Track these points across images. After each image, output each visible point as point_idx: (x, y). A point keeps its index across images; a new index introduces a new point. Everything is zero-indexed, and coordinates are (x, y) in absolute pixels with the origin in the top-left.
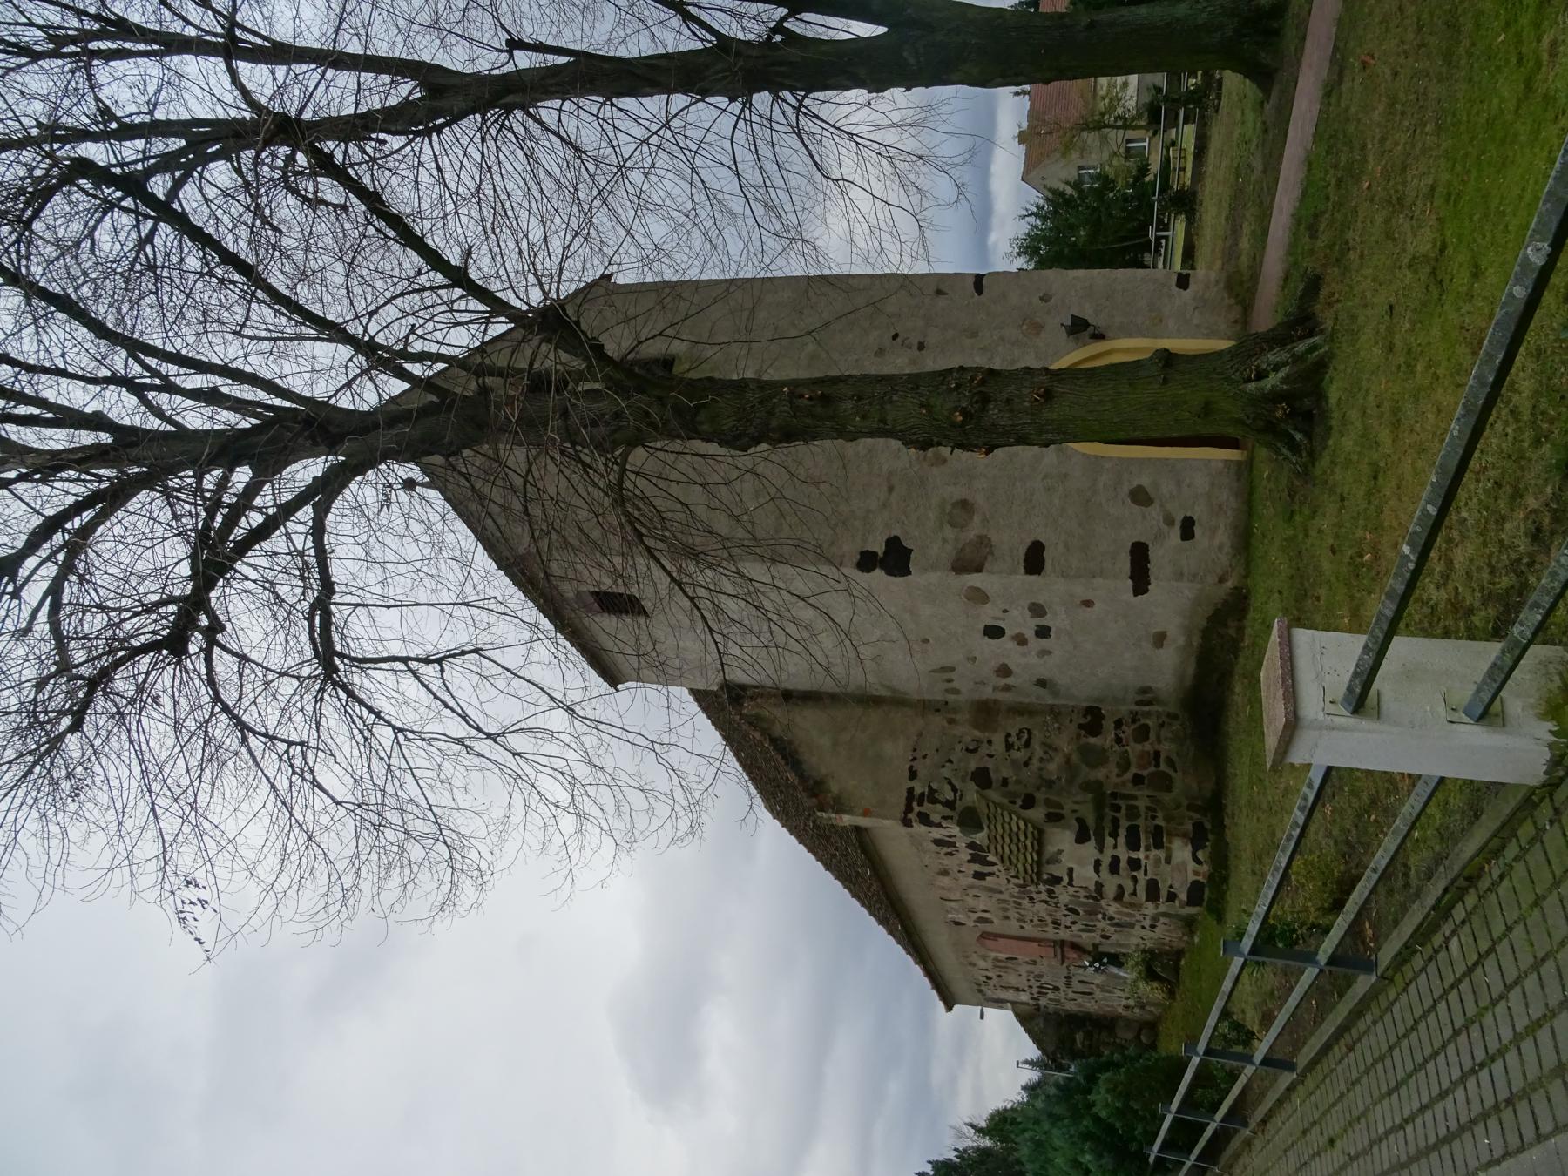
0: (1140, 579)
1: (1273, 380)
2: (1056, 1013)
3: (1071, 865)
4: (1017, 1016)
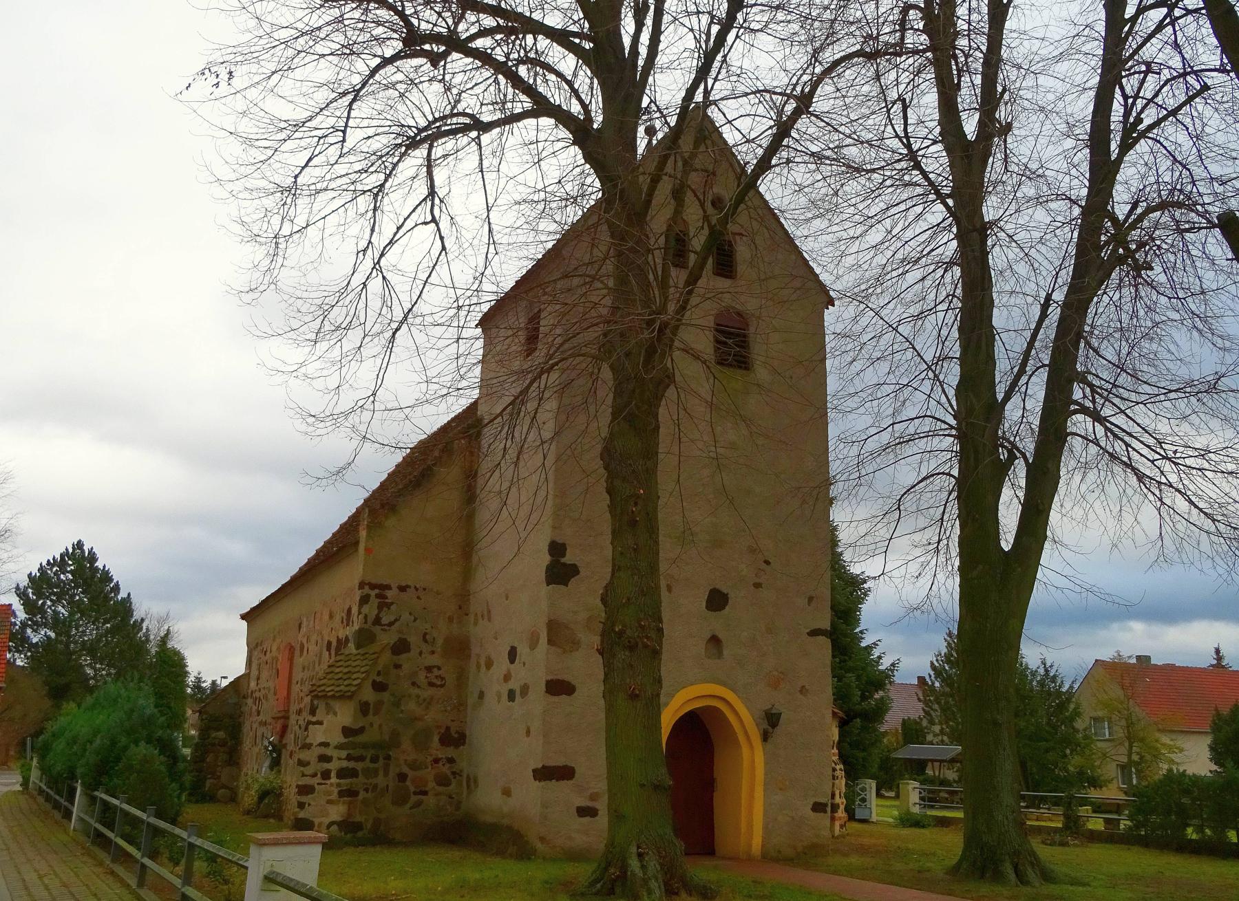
0: (546, 774)
1: (634, 864)
2: (241, 714)
3: (325, 722)
4: (238, 680)
